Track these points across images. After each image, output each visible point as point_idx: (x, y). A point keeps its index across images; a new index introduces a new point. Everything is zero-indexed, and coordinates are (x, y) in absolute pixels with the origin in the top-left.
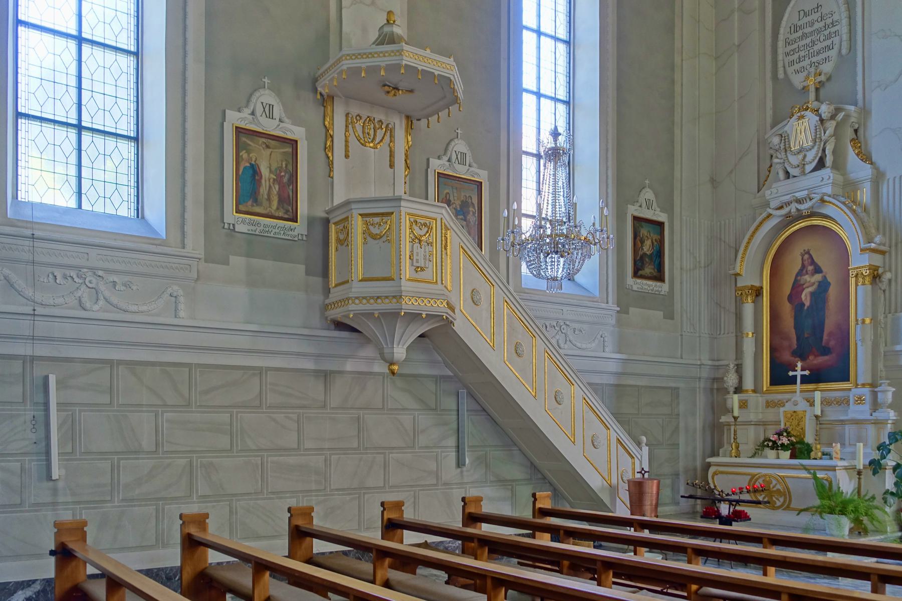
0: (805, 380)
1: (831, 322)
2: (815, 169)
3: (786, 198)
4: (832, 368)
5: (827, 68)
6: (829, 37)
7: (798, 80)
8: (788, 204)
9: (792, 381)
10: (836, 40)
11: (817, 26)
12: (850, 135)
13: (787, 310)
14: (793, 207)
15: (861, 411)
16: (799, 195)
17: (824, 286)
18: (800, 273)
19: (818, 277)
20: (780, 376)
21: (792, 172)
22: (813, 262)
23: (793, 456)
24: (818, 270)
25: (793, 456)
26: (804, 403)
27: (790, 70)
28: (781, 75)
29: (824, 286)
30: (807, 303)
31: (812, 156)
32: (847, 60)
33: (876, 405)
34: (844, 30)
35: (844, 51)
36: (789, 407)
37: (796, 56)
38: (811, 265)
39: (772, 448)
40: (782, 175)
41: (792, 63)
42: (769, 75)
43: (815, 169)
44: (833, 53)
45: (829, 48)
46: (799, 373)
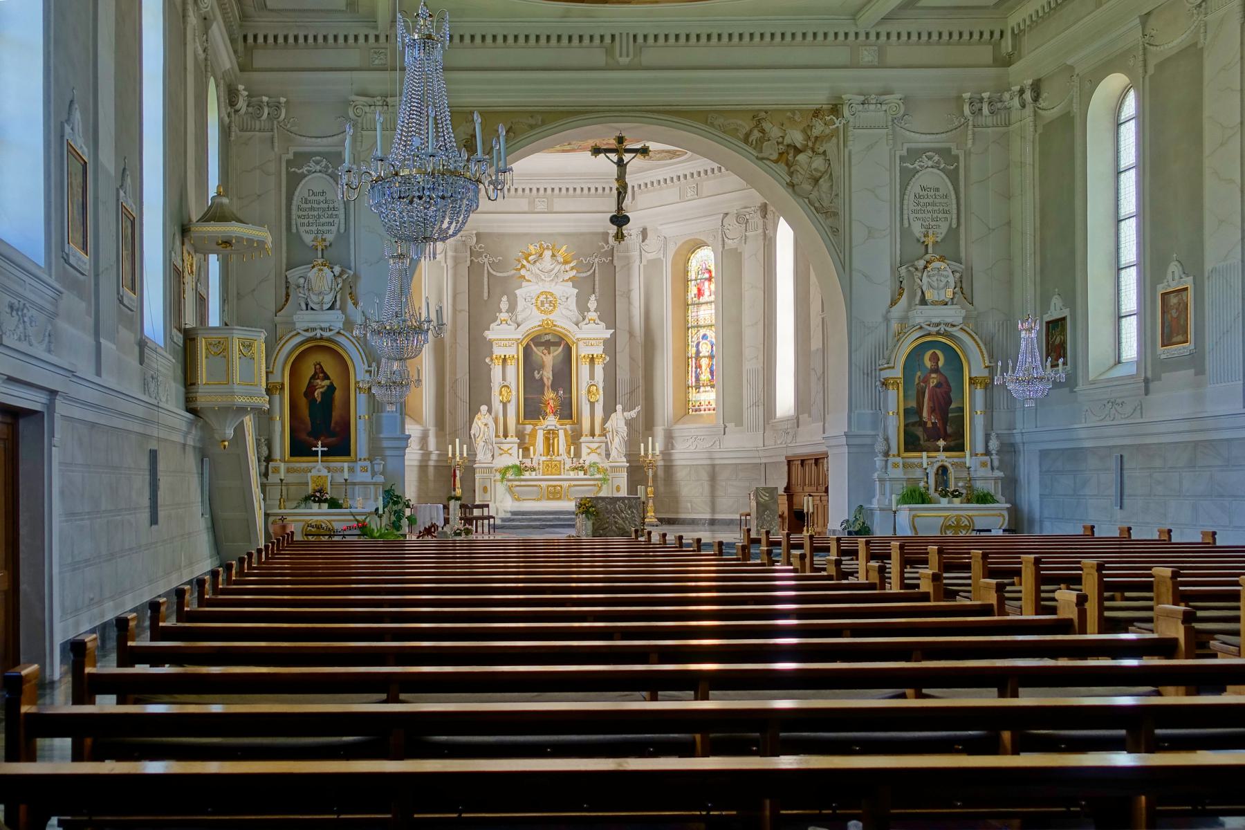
0: (324, 454)
1: (336, 414)
2: (330, 309)
3: (313, 325)
4: (340, 447)
5: (330, 238)
6: (331, 216)
7: (308, 239)
8: (314, 329)
9: (315, 454)
10: (336, 221)
11: (322, 205)
12: (348, 290)
13: (303, 403)
14: (319, 333)
15: (366, 477)
16: (323, 325)
17: (331, 388)
18: (313, 377)
19: (327, 382)
20: (300, 448)
21: (311, 305)
22: (323, 371)
23: (330, 507)
24: (326, 377)
25: (330, 507)
26: (318, 470)
27: (302, 229)
28: (294, 230)
29: (331, 388)
30: (319, 400)
31: (328, 299)
32: (344, 237)
33: (374, 474)
34: (342, 217)
35: (342, 231)
36: (314, 473)
37: (306, 221)
38: (320, 373)
39: (314, 501)
40: (304, 307)
41: (303, 225)
42: (284, 227)
43: (330, 309)
44: (334, 229)
45: (331, 224)
46: (320, 449)
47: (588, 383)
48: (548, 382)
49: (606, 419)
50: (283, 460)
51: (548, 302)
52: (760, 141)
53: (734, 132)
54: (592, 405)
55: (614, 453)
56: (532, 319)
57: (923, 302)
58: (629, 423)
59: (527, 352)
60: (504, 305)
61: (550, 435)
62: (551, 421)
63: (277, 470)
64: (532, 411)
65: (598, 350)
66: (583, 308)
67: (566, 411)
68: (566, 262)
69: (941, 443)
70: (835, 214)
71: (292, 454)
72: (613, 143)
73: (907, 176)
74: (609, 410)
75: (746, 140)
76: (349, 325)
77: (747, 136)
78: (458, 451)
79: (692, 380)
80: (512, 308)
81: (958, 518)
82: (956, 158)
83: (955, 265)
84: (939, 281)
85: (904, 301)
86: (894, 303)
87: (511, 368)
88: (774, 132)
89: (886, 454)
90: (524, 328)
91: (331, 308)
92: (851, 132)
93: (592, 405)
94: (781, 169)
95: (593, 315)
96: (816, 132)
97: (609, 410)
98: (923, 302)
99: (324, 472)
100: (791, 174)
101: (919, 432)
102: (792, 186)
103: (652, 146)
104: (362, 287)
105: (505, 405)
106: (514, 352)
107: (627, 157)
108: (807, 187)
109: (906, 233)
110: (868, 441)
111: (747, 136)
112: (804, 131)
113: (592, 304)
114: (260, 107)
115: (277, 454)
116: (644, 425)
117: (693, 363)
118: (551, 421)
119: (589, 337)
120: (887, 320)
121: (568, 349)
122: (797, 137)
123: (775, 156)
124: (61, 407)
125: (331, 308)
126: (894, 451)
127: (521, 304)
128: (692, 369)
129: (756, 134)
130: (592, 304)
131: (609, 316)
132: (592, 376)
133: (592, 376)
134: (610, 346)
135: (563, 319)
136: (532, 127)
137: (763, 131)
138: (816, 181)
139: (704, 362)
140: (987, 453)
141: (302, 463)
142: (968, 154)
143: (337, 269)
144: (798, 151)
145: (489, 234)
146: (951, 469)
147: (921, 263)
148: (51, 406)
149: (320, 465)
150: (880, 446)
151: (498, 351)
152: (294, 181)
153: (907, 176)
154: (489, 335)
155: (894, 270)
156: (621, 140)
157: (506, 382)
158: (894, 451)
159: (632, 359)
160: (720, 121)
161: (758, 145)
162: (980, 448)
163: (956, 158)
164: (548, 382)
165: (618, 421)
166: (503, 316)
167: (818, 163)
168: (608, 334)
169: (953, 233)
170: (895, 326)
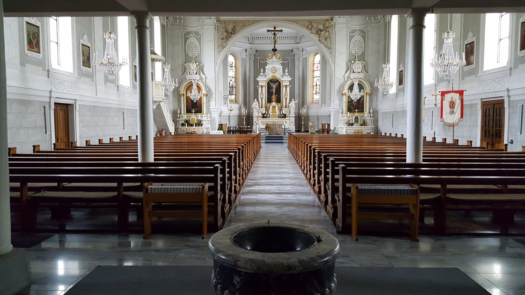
7: (190, 55)
31: (195, 71)
47: (285, 93)
48: (274, 93)
49: (289, 103)
50: (184, 114)
51: (274, 70)
52: (311, 28)
53: (304, 26)
54: (286, 99)
55: (291, 112)
56: (270, 75)
57: (354, 72)
58: (295, 104)
59: (268, 83)
60: (262, 71)
61: (274, 107)
62: (274, 104)
63: (182, 117)
64: (269, 101)
65: (288, 84)
66: (284, 71)
67: (278, 101)
68: (279, 59)
69: (357, 110)
70: (331, 48)
71: (187, 112)
72: (273, 29)
73: (351, 38)
74: (290, 100)
75: (307, 28)
76: (201, 79)
77: (308, 27)
78: (304, 111)
79: (315, 92)
80: (264, 72)
81: (358, 130)
82: (365, 32)
83: (363, 62)
84: (358, 66)
85: (348, 72)
86: (346, 72)
87: (264, 89)
88: (315, 26)
89: (342, 113)
90: (267, 77)
91: (196, 74)
92: (336, 25)
93: (286, 99)
94: (317, 36)
95: (287, 74)
96: (326, 26)
97: (290, 100)
98: (354, 72)
99: (195, 117)
100: (319, 37)
101: (352, 107)
102: (319, 40)
103: (283, 29)
104: (205, 69)
105: (262, 99)
106: (265, 84)
107: (276, 33)
108: (324, 41)
109: (350, 53)
110: (338, 110)
111: (308, 27)
112: (323, 25)
113: (287, 71)
114: (176, 19)
115: (183, 113)
116: (302, 103)
117: (315, 87)
118: (274, 104)
119: (285, 80)
120: (344, 77)
121: (280, 83)
122: (321, 27)
123: (315, 32)
124: (78, 103)
125: (196, 74)
126: (344, 112)
127: (267, 70)
128: (315, 89)
129: (310, 26)
130: (287, 71)
131: (292, 74)
132: (286, 91)
133: (286, 91)
134: (292, 83)
135: (278, 75)
136: (250, 25)
137: (312, 25)
138: (326, 39)
139: (318, 87)
140: (370, 113)
141: (189, 115)
142: (368, 31)
143: (197, 64)
144: (321, 31)
145: (260, 51)
146: (359, 117)
147: (353, 62)
148: (75, 103)
149: (193, 115)
150: (341, 111)
151: (260, 84)
152: (186, 39)
153: (351, 38)
154: (258, 79)
155: (347, 64)
156: (275, 28)
157: (263, 93)
158: (344, 112)
159: (299, 86)
160: (301, 23)
161: (311, 29)
162: (368, 112)
163: (365, 32)
164: (274, 93)
165: (293, 104)
166: (262, 74)
167: (327, 34)
168: (290, 79)
169: (363, 53)
170: (346, 79)
